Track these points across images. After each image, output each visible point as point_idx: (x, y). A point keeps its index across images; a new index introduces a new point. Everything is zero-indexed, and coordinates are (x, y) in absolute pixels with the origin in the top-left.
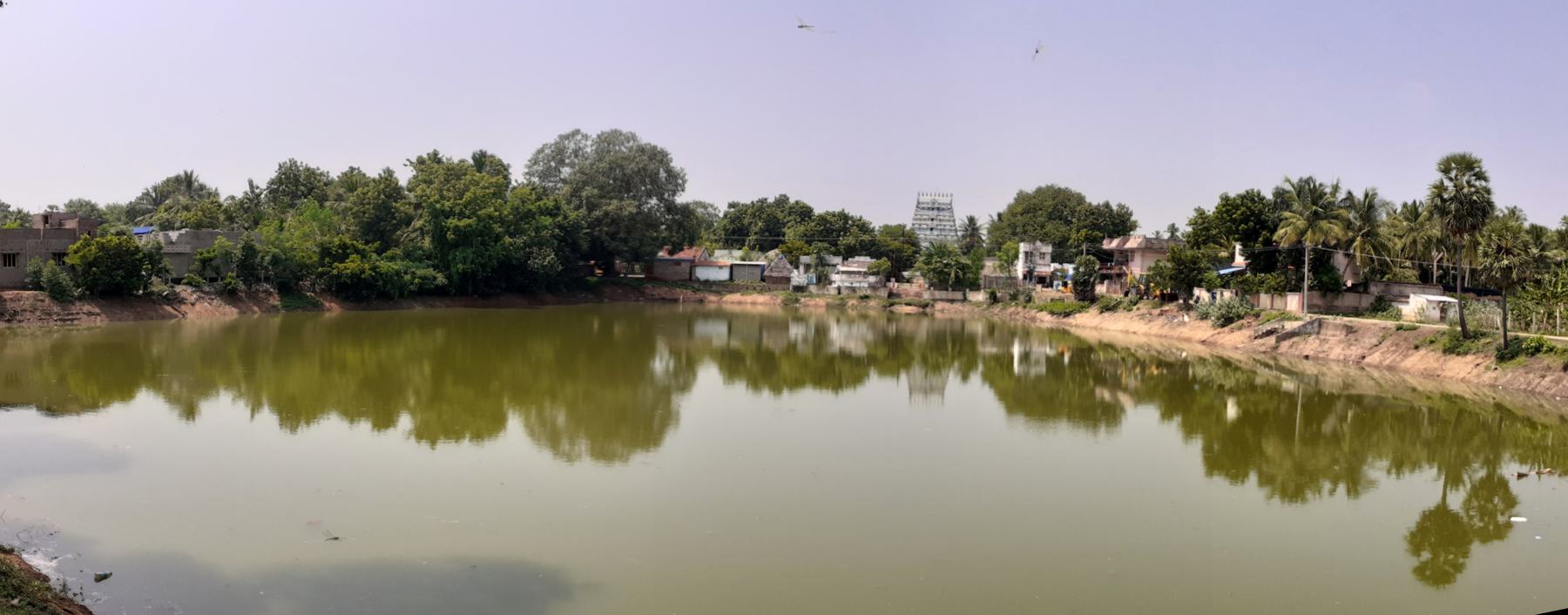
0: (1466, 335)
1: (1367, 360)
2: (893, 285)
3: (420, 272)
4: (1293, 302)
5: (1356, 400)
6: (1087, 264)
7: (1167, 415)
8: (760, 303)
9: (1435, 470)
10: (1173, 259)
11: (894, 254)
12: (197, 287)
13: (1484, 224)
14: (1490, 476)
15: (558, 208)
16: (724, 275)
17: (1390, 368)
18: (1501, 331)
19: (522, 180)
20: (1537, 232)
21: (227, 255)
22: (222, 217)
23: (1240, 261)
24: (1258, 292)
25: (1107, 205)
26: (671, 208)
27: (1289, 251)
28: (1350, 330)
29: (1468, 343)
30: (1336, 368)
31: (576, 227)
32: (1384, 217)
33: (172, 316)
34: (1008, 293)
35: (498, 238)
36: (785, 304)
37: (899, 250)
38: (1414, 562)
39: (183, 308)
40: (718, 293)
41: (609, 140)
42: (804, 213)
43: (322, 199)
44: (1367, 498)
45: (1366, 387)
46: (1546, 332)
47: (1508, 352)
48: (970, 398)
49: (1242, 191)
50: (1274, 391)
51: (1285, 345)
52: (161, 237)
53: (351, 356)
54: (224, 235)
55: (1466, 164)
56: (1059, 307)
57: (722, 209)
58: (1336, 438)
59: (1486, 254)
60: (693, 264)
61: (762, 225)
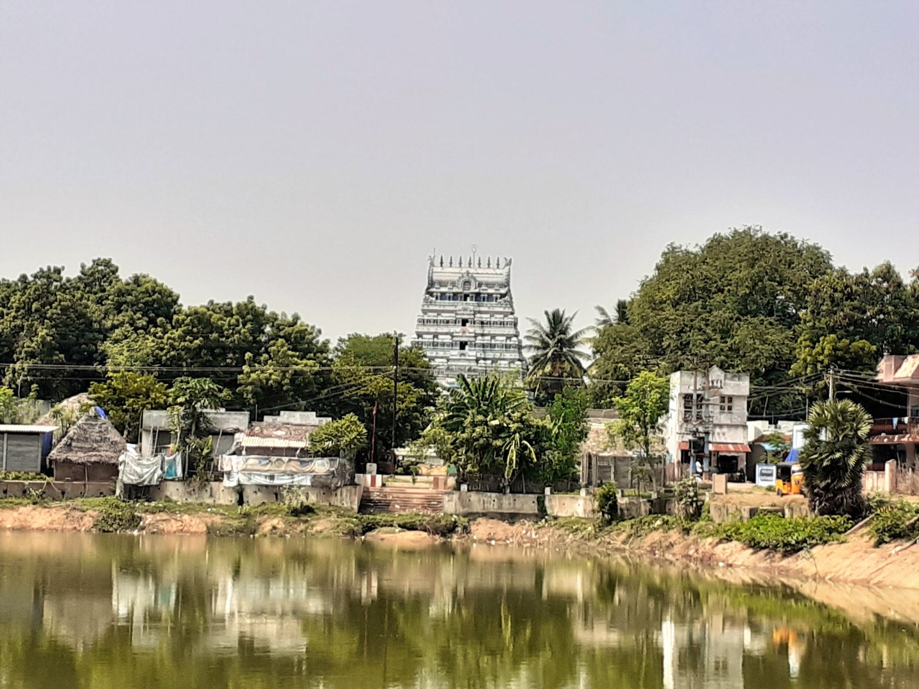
2: (372, 479)
6: (839, 421)
11: (374, 407)
25: (887, 273)
34: (649, 497)
36: (103, 529)
37: (387, 397)
42: (157, 305)
56: (769, 532)
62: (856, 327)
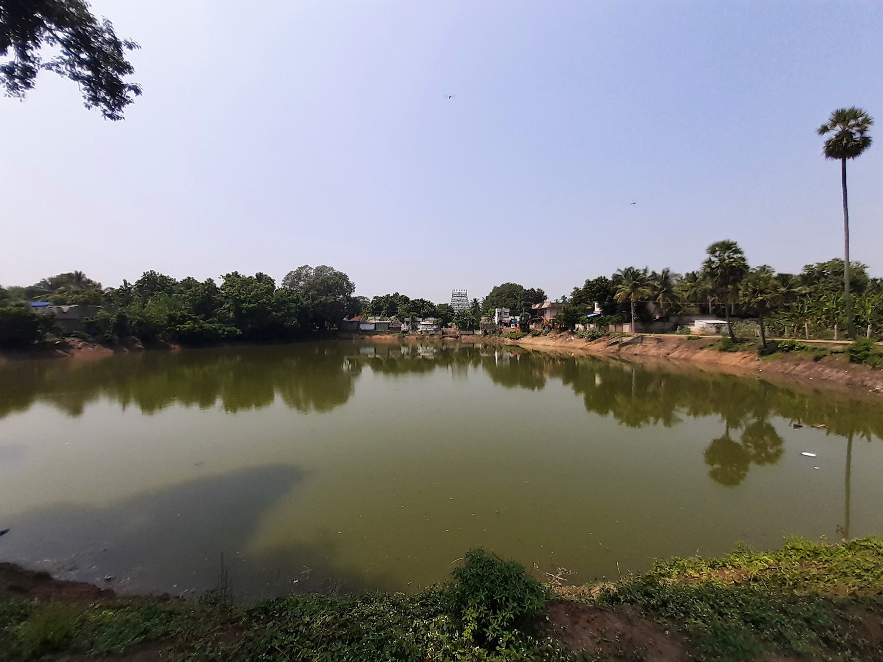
0: (734, 340)
1: (671, 355)
2: (444, 329)
3: (227, 329)
4: (626, 328)
5: (667, 376)
6: (525, 316)
7: (566, 382)
8: (388, 338)
9: (720, 415)
10: (564, 312)
11: (443, 315)
12: (83, 339)
13: (742, 278)
14: (760, 424)
15: (298, 299)
16: (372, 327)
17: (685, 359)
18: (761, 338)
19: (281, 286)
20: (784, 278)
21: (106, 320)
22: (103, 299)
23: (597, 310)
24: (608, 325)
25: (532, 289)
26: (349, 299)
27: (623, 304)
28: (659, 340)
29: (737, 345)
30: (653, 360)
31: (307, 308)
32: (675, 282)
33: (62, 356)
34: (494, 330)
35: (270, 312)
36: (399, 338)
37: (446, 314)
38: (709, 468)
39: (72, 351)
40: (369, 335)
41: (321, 270)
42: (406, 300)
43: (170, 292)
44: (676, 428)
45: (671, 368)
46: (797, 337)
47: (767, 350)
48: (478, 377)
49: (596, 278)
50: (619, 370)
51: (624, 348)
52: (55, 309)
53: (187, 371)
54: (105, 309)
55: (727, 246)
56: (514, 336)
57: (371, 299)
58: (655, 395)
59: (745, 295)
60: (359, 323)
61: (390, 306)
62: (528, 299)
